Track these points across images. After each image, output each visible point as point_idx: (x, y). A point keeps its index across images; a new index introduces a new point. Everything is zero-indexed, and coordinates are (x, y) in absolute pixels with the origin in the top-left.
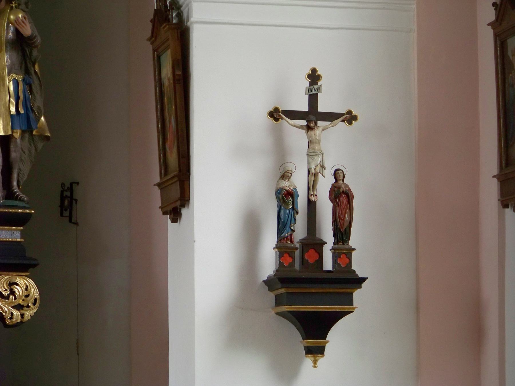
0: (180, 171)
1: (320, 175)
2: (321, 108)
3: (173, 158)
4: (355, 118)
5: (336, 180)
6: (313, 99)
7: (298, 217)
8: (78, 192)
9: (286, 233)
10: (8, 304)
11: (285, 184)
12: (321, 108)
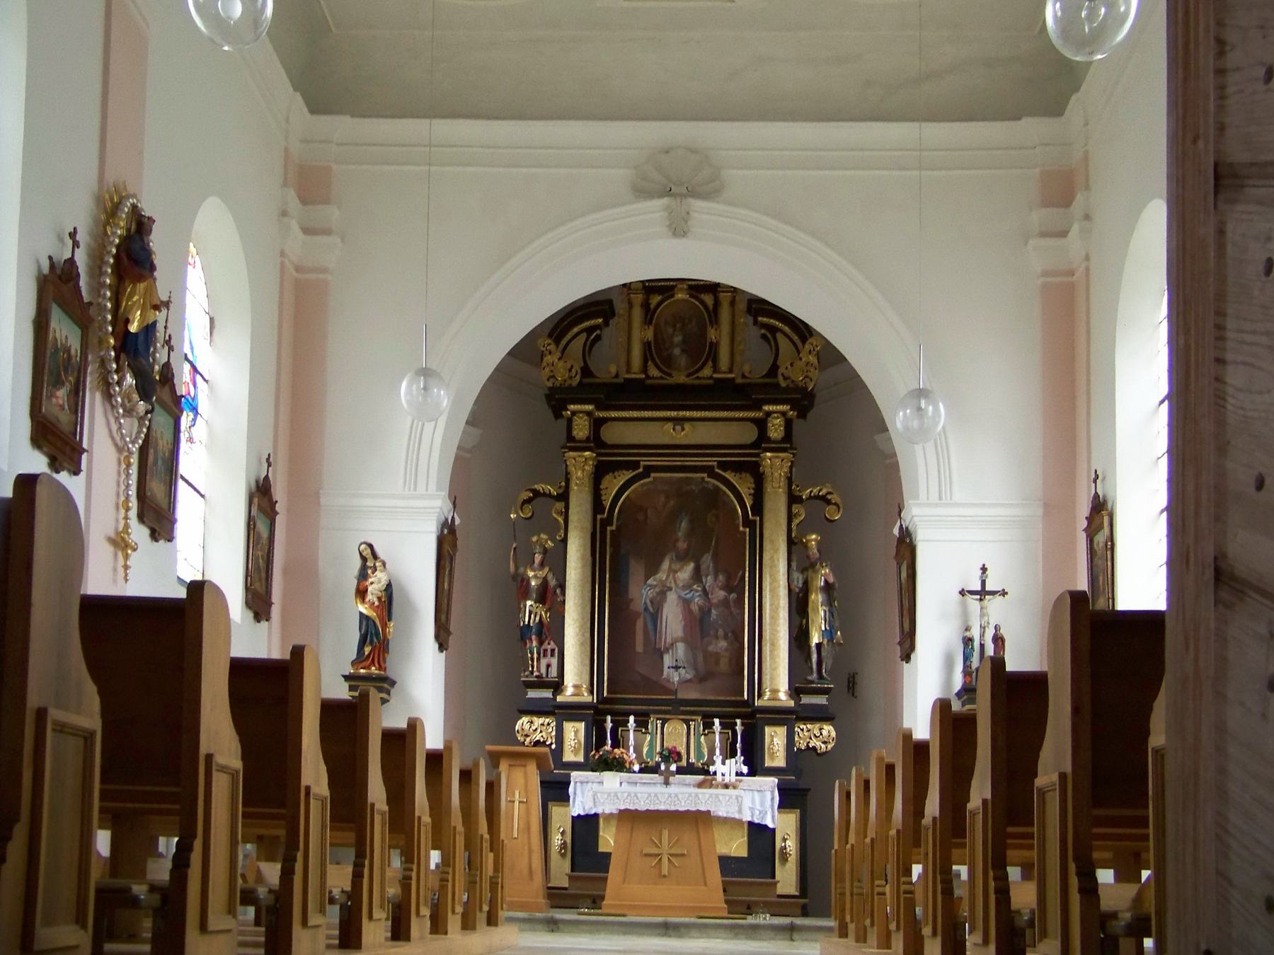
0: (910, 629)
1: (987, 628)
2: (988, 588)
3: (907, 626)
4: (1007, 593)
5: (996, 631)
6: (983, 583)
7: (974, 654)
8: (858, 679)
9: (968, 663)
10: (819, 741)
11: (968, 634)
12: (988, 588)
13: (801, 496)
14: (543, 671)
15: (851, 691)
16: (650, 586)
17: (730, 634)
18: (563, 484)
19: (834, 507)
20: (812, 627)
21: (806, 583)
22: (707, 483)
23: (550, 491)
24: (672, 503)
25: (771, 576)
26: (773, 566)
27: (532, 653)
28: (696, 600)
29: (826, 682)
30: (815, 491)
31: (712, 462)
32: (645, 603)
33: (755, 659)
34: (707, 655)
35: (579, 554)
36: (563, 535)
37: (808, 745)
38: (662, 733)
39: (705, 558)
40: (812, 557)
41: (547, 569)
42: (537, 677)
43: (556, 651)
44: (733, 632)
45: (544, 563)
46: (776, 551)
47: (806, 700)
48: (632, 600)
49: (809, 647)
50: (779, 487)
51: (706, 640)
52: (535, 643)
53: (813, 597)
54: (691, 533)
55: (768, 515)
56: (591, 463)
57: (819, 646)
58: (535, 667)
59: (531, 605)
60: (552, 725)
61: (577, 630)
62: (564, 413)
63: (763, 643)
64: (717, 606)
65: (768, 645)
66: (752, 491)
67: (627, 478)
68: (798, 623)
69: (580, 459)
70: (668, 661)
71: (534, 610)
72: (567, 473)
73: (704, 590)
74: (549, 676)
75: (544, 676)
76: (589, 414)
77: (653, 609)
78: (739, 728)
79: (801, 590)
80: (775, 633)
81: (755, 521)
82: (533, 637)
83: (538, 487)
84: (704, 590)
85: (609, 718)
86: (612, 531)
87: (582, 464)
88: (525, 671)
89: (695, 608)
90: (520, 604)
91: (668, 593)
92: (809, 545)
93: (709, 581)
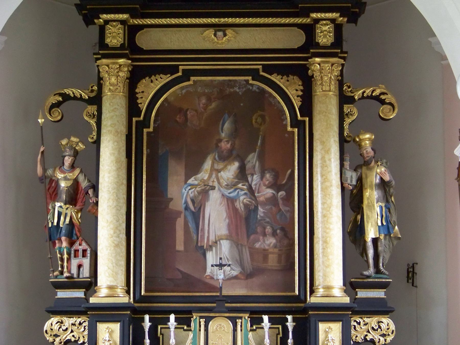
13: (353, 97)
14: (74, 271)
15: (411, 281)
16: (190, 185)
17: (278, 231)
18: (95, 88)
19: (389, 107)
20: (368, 222)
21: (360, 180)
22: (252, 85)
23: (81, 95)
24: (214, 105)
25: (322, 176)
26: (324, 166)
27: (62, 254)
28: (242, 198)
29: (385, 276)
30: (368, 91)
31: (258, 66)
32: (186, 202)
33: (324, 314)
34: (253, 252)
35: (113, 158)
36: (95, 137)
37: (365, 339)
38: (206, 330)
39: (251, 156)
40: (365, 155)
41: (77, 171)
42: (67, 278)
43: (89, 252)
44: (283, 229)
45: (74, 165)
46: (328, 151)
47: (362, 294)
48: (171, 199)
49: (365, 242)
50: (330, 91)
51: (252, 237)
52: (65, 244)
53: (367, 194)
54: (234, 134)
55: (317, 118)
56: (126, 69)
57: (375, 241)
58: (65, 267)
59: (61, 207)
60: (84, 324)
61: (112, 232)
62: (96, 21)
63: (315, 240)
64: (263, 204)
65: (321, 242)
66: (300, 93)
67: (165, 82)
68: (352, 218)
69: (114, 66)
70: (211, 258)
71: (64, 211)
72: (100, 79)
73: (250, 188)
74: (81, 276)
75: (75, 276)
76: (123, 22)
77: (195, 208)
78: (290, 325)
79: (355, 186)
80: (328, 231)
81: (304, 122)
82: (63, 238)
83: (67, 91)
84: (250, 188)
85: (147, 317)
86: (148, 133)
87: (117, 70)
88: (53, 271)
89: (239, 206)
90: (47, 204)
91: (211, 192)
92: (363, 144)
93: (255, 180)
